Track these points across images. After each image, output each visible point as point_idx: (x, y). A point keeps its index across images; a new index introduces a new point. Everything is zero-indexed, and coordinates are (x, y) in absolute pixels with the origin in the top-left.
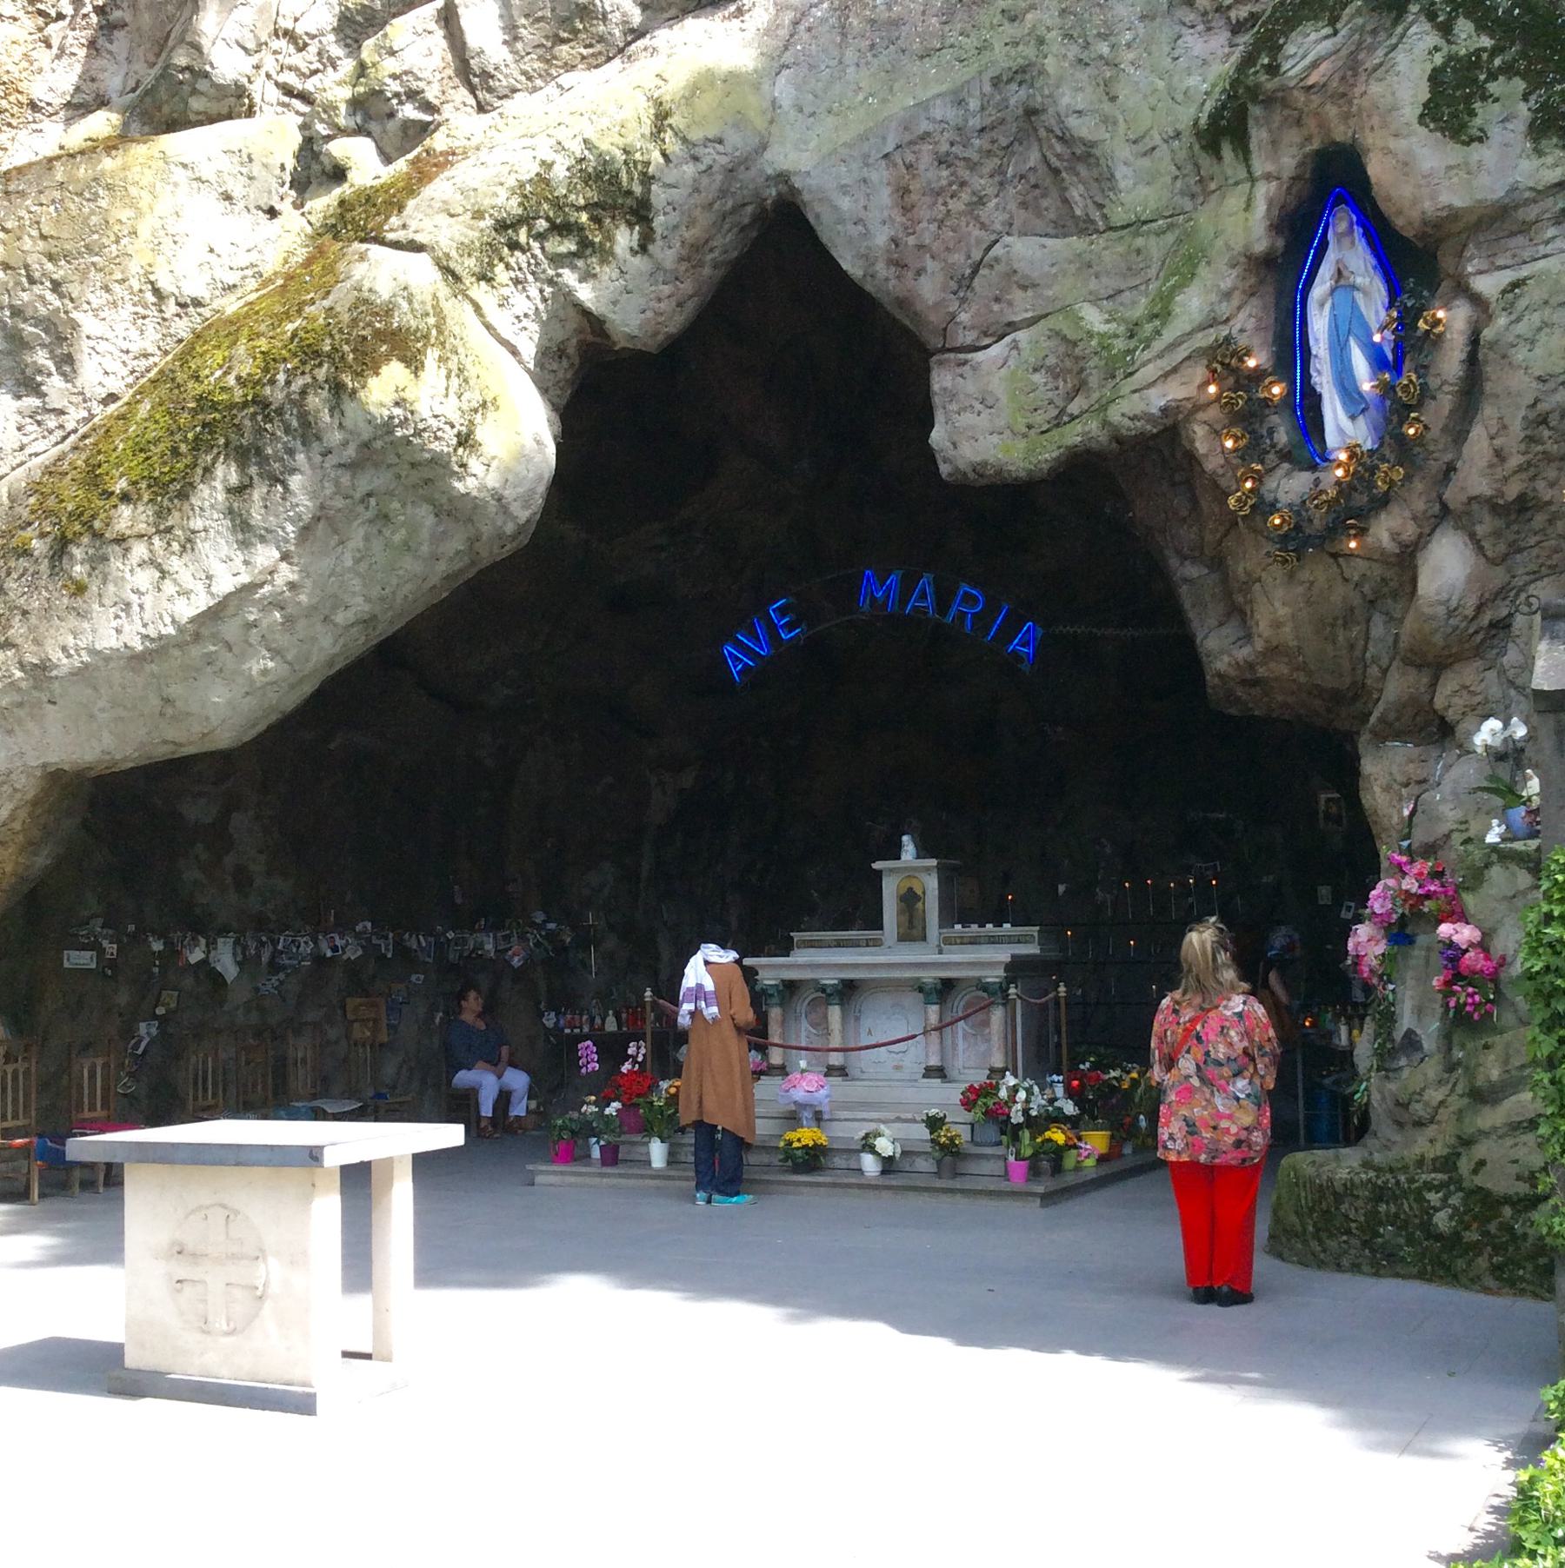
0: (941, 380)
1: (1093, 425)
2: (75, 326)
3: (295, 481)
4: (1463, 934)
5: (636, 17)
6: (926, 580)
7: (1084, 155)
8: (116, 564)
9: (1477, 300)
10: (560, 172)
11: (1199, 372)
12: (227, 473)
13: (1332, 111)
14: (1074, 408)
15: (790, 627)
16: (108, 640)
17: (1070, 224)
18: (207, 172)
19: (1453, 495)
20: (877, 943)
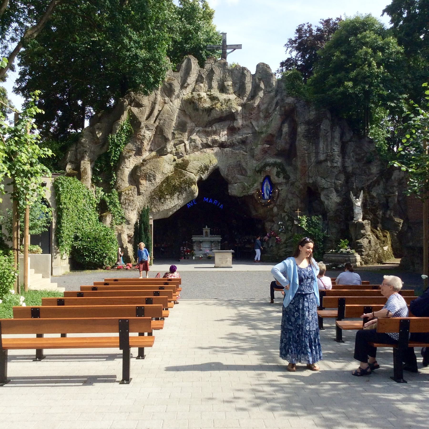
0: (229, 186)
1: (246, 194)
2: (156, 175)
3: (184, 194)
4: (278, 238)
5: (201, 148)
7: (245, 169)
8: (167, 201)
9: (278, 190)
10: (203, 166)
12: (178, 193)
14: (244, 191)
15: (195, 203)
16: (165, 208)
17: (242, 174)
18: (167, 161)
19: (276, 204)
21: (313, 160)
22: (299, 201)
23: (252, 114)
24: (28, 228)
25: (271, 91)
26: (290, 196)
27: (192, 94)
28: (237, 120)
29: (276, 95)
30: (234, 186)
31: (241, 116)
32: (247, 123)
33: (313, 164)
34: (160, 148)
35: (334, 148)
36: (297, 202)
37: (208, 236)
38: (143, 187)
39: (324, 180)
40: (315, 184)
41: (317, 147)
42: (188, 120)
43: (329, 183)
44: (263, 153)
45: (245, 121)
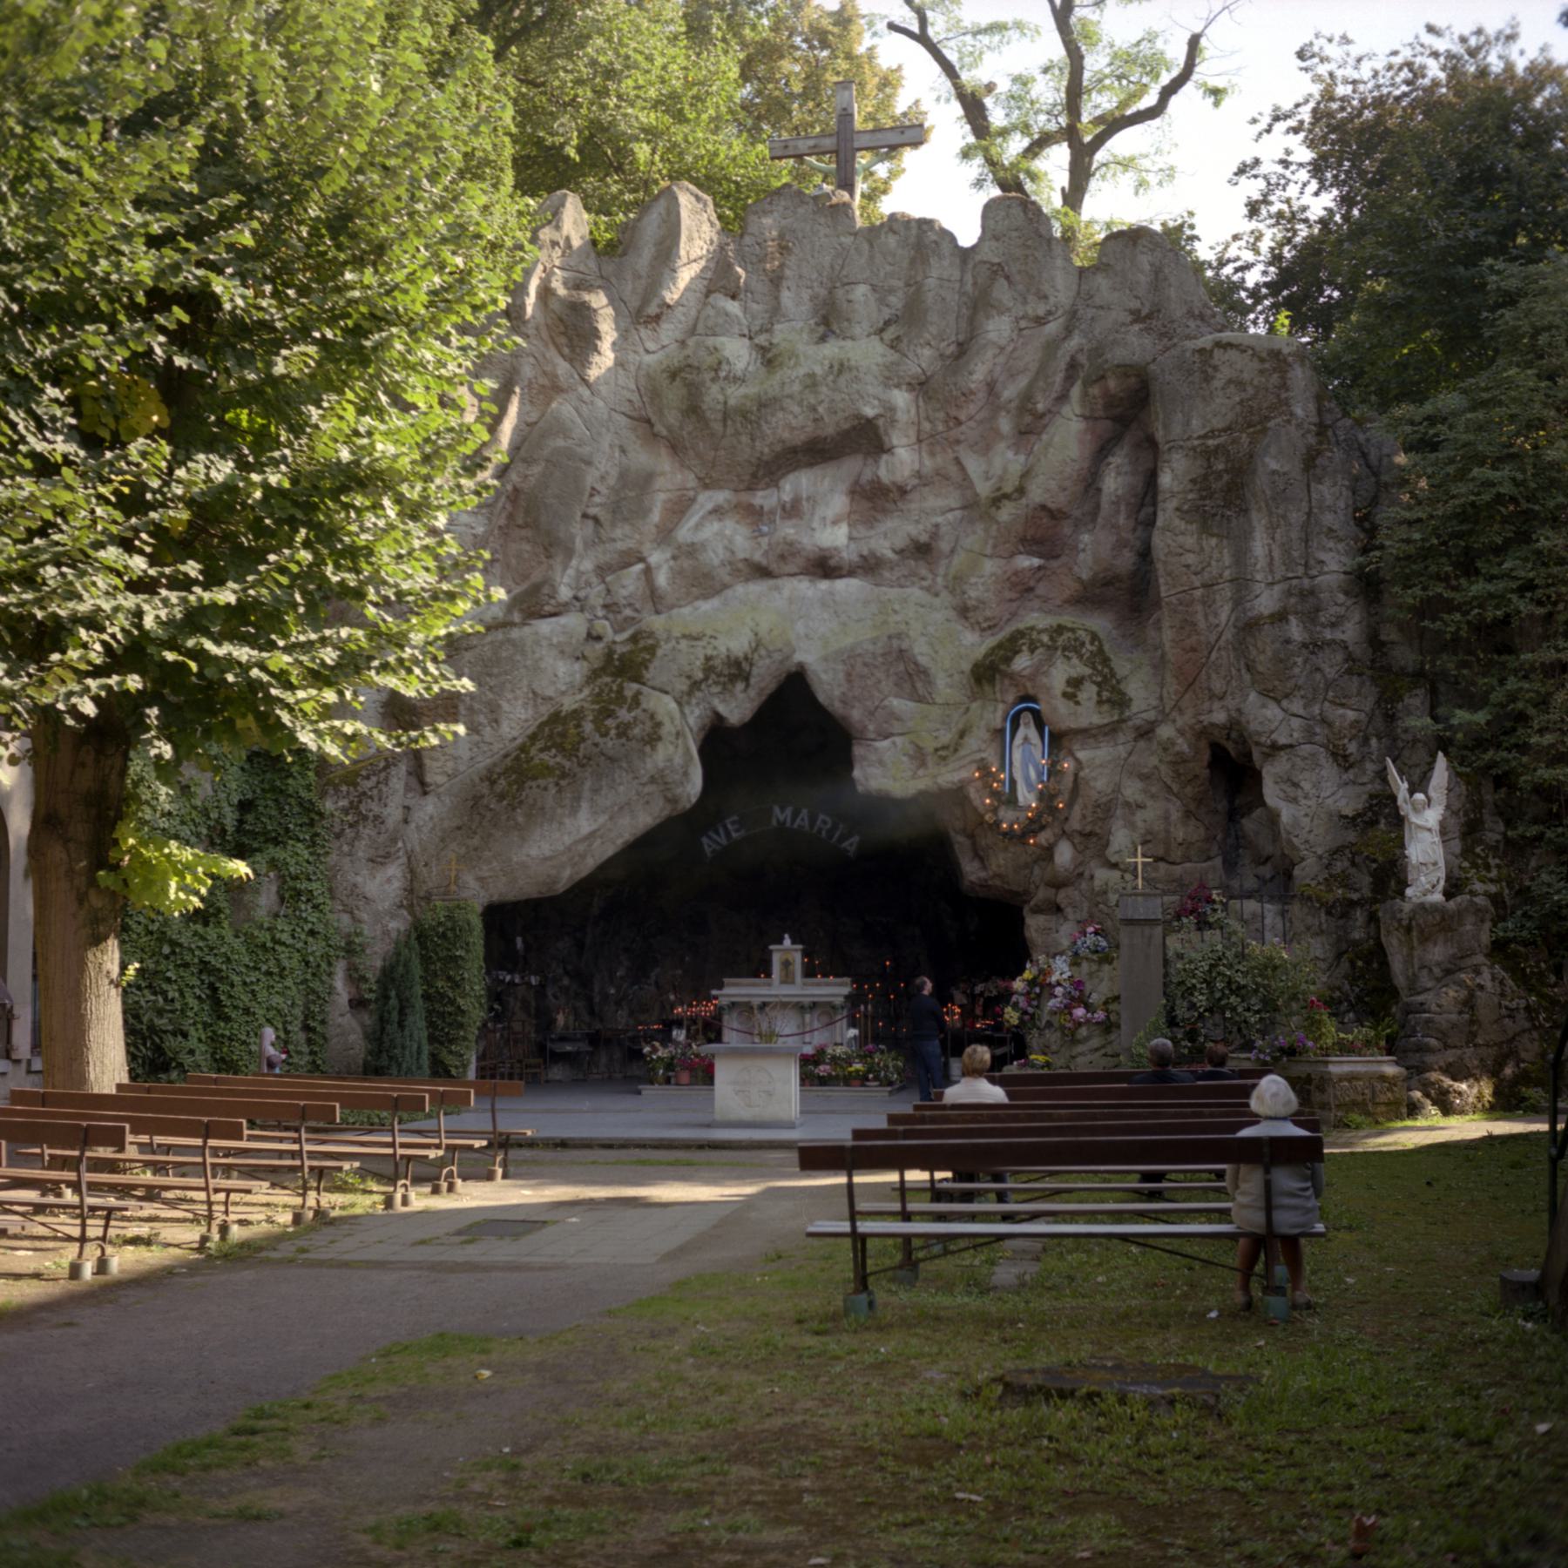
0: (858, 750)
2: (499, 706)
6: (805, 812)
7: (924, 672)
9: (1077, 760)
11: (974, 766)
13: (1029, 684)
19: (1067, 828)
20: (769, 985)
21: (1223, 617)
22: (1175, 815)
23: (959, 423)
24: (1123, 1027)
25: (1050, 313)
26: (1132, 790)
27: (683, 343)
28: (890, 450)
29: (1068, 331)
30: (876, 749)
31: (912, 433)
32: (942, 460)
33: (1228, 635)
34: (524, 586)
35: (1322, 556)
36: (1167, 818)
37: (793, 982)
38: (437, 760)
39: (1277, 711)
40: (1234, 726)
41: (1241, 556)
42: (664, 463)
43: (1296, 722)
44: (1008, 595)
45: (932, 454)
